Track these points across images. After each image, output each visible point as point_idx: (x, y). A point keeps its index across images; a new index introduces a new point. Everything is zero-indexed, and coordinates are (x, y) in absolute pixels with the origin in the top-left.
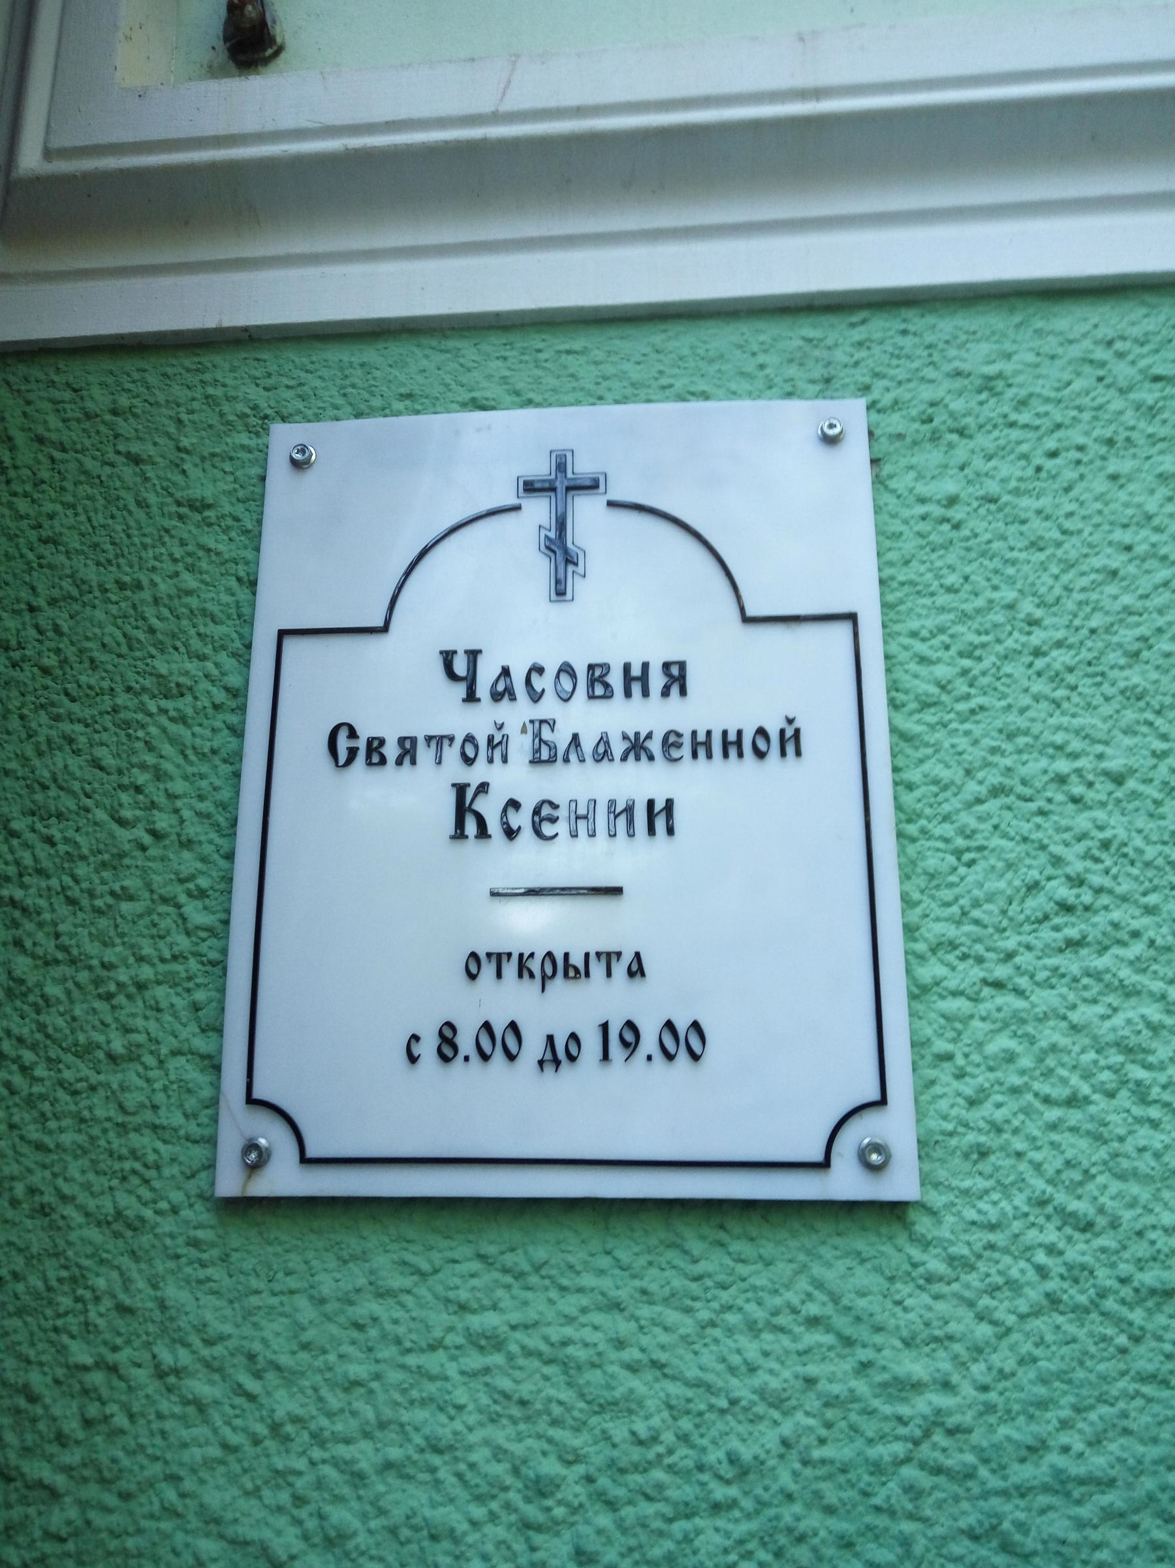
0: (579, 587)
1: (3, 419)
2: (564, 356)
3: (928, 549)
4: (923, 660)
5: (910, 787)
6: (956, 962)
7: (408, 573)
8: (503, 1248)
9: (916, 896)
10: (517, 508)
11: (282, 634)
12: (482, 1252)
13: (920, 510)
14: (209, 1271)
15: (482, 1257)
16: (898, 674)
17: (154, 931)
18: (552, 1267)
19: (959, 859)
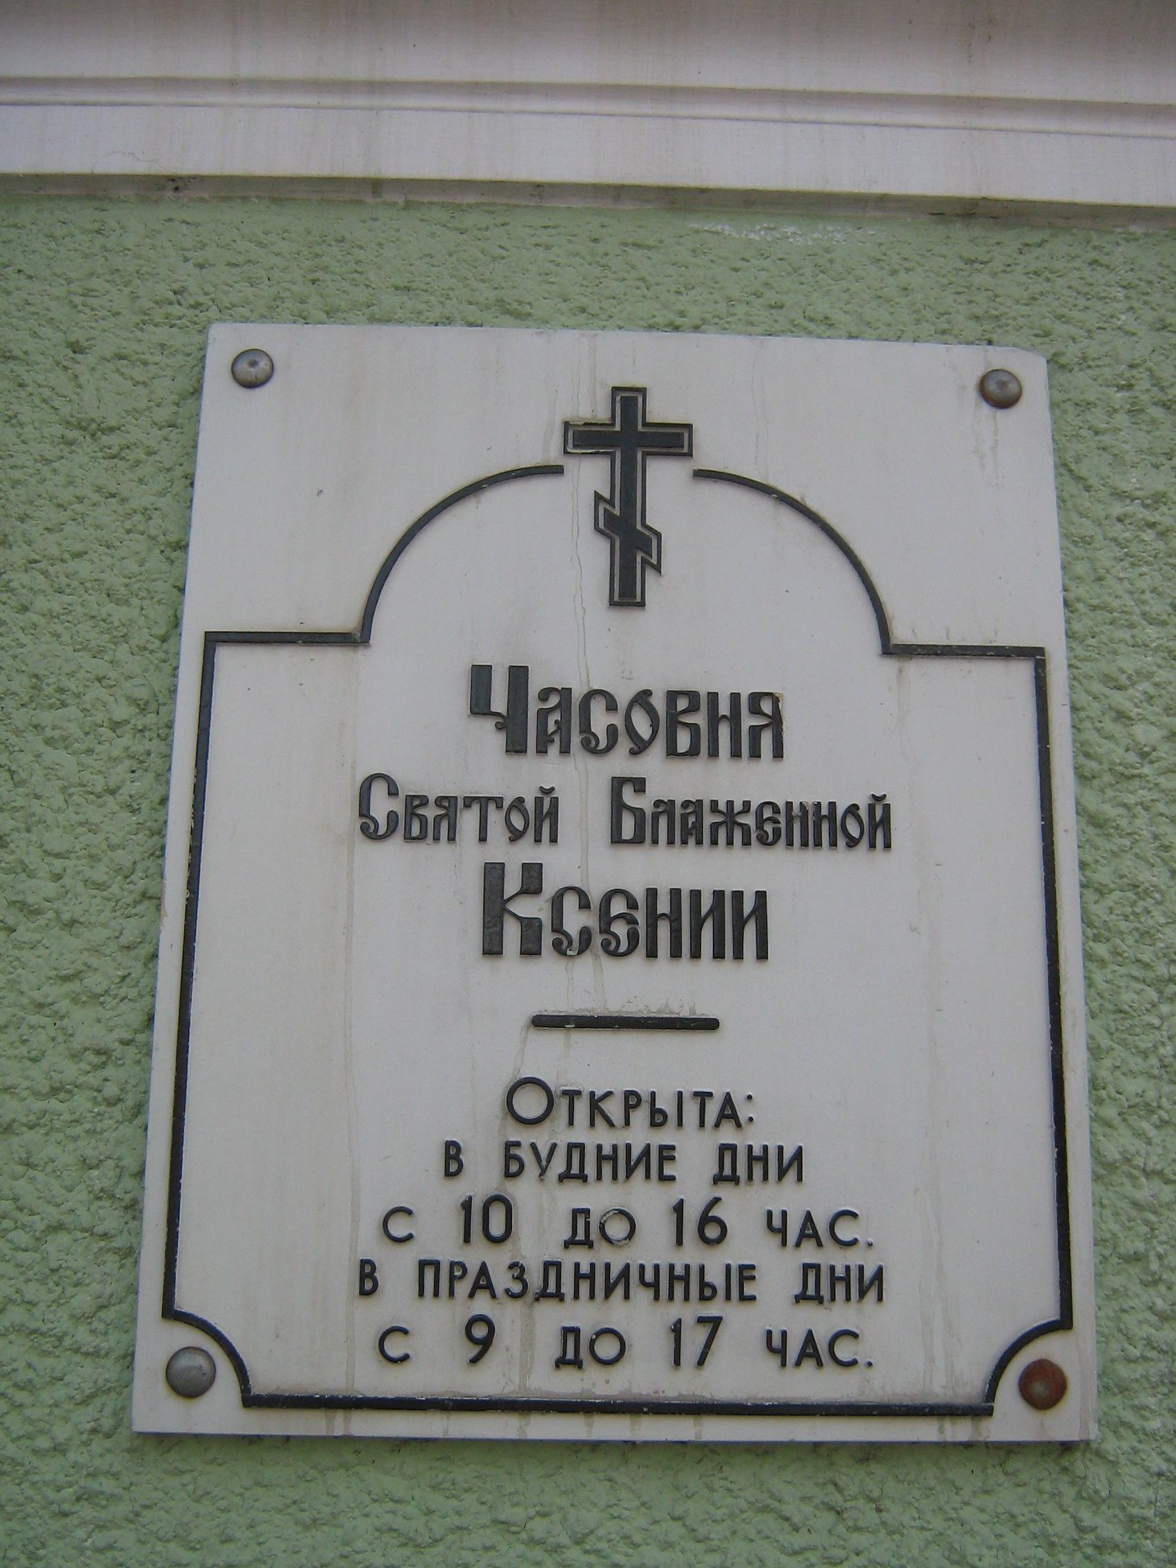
0: (654, 588)
1: (998, 1566)
2: (631, 250)
3: (1126, 564)
4: (1121, 716)
5: (1102, 891)
6: (1152, 1132)
7: (785, 500)
8: (532, 1512)
9: (1105, 1042)
10: (557, 470)
11: (213, 641)
12: (502, 1517)
13: (1118, 509)
14: (113, 1534)
15: (503, 1525)
16: (1090, 735)
17: (23, 1050)
18: (600, 1539)
19: (1160, 992)
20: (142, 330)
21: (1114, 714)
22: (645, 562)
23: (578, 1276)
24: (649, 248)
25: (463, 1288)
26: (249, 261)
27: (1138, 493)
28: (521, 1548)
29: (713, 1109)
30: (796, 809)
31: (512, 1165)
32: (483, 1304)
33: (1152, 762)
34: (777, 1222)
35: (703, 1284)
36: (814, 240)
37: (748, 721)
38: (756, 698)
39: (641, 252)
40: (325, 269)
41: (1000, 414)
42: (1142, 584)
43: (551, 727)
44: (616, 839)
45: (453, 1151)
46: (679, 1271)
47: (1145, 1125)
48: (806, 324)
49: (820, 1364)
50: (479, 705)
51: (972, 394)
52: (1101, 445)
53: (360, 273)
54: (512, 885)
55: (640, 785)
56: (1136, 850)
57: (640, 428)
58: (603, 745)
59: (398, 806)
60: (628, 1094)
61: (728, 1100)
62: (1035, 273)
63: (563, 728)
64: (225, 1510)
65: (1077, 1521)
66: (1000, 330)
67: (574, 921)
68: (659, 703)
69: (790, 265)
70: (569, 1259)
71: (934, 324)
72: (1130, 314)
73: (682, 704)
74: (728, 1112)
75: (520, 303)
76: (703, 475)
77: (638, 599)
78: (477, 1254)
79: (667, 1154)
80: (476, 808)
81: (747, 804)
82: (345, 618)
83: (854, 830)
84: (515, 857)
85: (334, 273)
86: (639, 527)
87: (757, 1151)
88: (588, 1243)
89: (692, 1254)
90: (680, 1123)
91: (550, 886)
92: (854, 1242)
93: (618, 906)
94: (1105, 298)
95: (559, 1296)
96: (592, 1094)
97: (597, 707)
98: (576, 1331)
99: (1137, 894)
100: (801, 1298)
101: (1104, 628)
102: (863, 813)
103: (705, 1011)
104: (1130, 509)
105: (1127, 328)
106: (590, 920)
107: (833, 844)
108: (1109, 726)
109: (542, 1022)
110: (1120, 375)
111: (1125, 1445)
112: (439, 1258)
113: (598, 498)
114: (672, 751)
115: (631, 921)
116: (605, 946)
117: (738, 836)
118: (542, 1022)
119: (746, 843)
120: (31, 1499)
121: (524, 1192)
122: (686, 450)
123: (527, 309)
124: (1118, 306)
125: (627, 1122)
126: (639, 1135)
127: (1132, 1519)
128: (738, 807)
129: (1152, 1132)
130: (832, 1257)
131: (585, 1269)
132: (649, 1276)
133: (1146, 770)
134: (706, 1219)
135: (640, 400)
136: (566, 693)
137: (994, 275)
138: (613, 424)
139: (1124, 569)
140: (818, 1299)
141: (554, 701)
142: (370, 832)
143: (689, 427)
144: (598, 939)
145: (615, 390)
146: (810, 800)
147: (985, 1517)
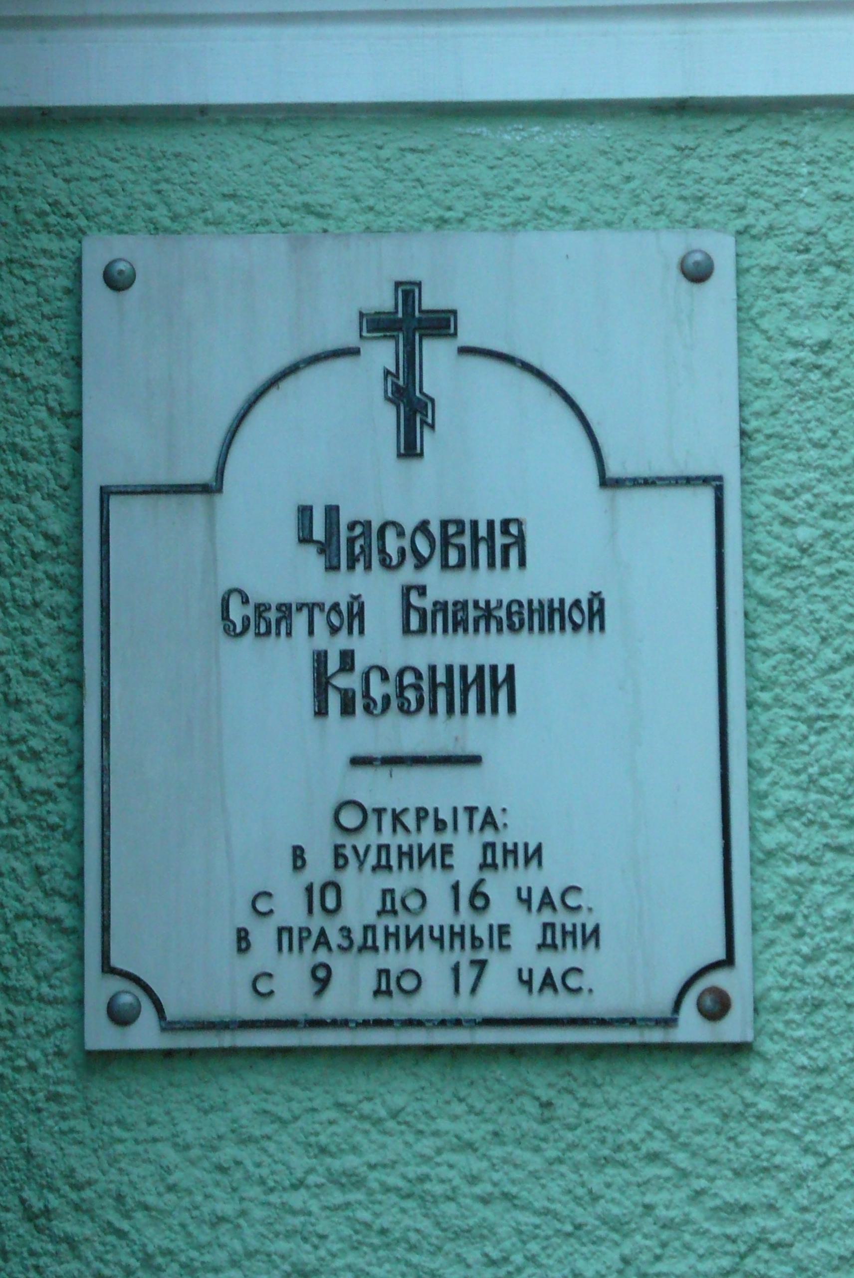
0: (429, 441)
3: (796, 399)
4: (786, 521)
6: (802, 829)
8: (361, 1097)
10: (354, 352)
11: (106, 493)
13: (791, 355)
14: (72, 1123)
16: (761, 536)
18: (408, 1114)
20: (27, 238)
21: (781, 519)
22: (423, 422)
23: (387, 935)
24: (422, 152)
25: (309, 945)
26: (106, 175)
27: (808, 342)
28: (354, 1122)
29: (478, 819)
30: (536, 605)
31: (339, 859)
32: (322, 955)
33: (810, 556)
34: (524, 895)
35: (474, 938)
36: (554, 137)
37: (500, 540)
38: (506, 523)
39: (416, 155)
40: (167, 181)
41: (696, 287)
42: (808, 415)
43: (357, 550)
44: (406, 629)
45: (298, 852)
46: (457, 929)
47: (796, 824)
48: (547, 212)
49: (555, 990)
50: (305, 539)
51: (675, 272)
52: (782, 301)
53: (195, 183)
54: (333, 664)
55: (422, 591)
56: (796, 623)
57: (417, 314)
58: (394, 562)
59: (250, 611)
60: (419, 810)
61: (489, 812)
62: (734, 156)
63: (366, 550)
64: (148, 1104)
65: (743, 1098)
66: (703, 208)
67: (377, 690)
68: (435, 529)
69: (535, 160)
70: (380, 924)
71: (650, 206)
72: (811, 186)
73: (452, 529)
74: (489, 820)
75: (322, 206)
76: (465, 351)
77: (418, 450)
78: (317, 922)
79: (447, 849)
80: (305, 611)
81: (500, 603)
82: (205, 474)
83: (577, 618)
84: (334, 646)
85: (174, 184)
86: (418, 394)
87: (510, 847)
88: (394, 912)
89: (466, 916)
90: (455, 828)
91: (360, 664)
92: (579, 908)
93: (409, 679)
94: (790, 174)
95: (375, 948)
96: (394, 810)
97: (390, 534)
98: (387, 972)
99: (795, 655)
100: (542, 946)
101: (778, 452)
102: (585, 606)
103: (471, 749)
104: (802, 354)
105: (808, 200)
106: (390, 689)
107: (563, 628)
108: (777, 528)
109: (358, 761)
110: (800, 242)
111: (777, 1048)
112: (292, 925)
113: (387, 373)
114: (445, 565)
115: (417, 688)
116: (401, 708)
117: (493, 626)
118: (358, 761)
119: (500, 630)
120: (14, 1101)
121: (349, 878)
122: (452, 330)
123: (328, 210)
124: (801, 180)
125: (419, 829)
126: (427, 837)
127: (783, 1098)
128: (493, 604)
129: (802, 829)
130: (561, 918)
131: (392, 929)
132: (436, 933)
133: (805, 561)
134: (476, 893)
135: (417, 291)
136: (367, 525)
137: (702, 159)
138: (396, 312)
139: (795, 404)
140: (554, 946)
141: (358, 530)
142: (231, 631)
143: (454, 313)
144: (394, 703)
145: (398, 284)
146: (545, 596)
147: (677, 1097)
